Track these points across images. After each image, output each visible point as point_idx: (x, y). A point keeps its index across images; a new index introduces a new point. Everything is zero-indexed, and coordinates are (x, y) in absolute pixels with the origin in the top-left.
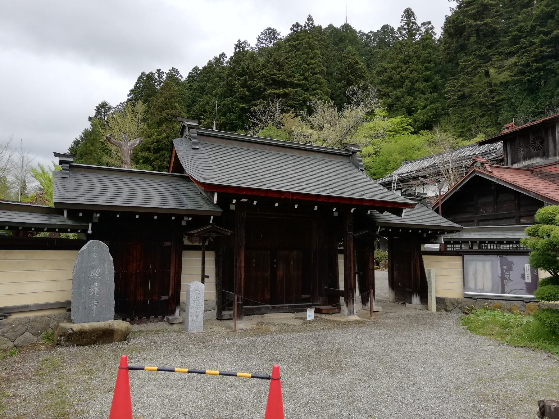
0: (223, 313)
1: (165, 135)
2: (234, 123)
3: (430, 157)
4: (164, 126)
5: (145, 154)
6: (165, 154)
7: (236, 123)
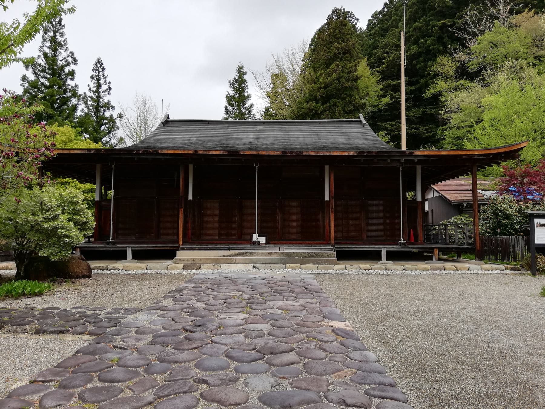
0: (78, 250)
1: (334, 75)
2: (431, 51)
3: (518, 270)
4: (333, 66)
5: (312, 105)
6: (336, 103)
7: (434, 49)
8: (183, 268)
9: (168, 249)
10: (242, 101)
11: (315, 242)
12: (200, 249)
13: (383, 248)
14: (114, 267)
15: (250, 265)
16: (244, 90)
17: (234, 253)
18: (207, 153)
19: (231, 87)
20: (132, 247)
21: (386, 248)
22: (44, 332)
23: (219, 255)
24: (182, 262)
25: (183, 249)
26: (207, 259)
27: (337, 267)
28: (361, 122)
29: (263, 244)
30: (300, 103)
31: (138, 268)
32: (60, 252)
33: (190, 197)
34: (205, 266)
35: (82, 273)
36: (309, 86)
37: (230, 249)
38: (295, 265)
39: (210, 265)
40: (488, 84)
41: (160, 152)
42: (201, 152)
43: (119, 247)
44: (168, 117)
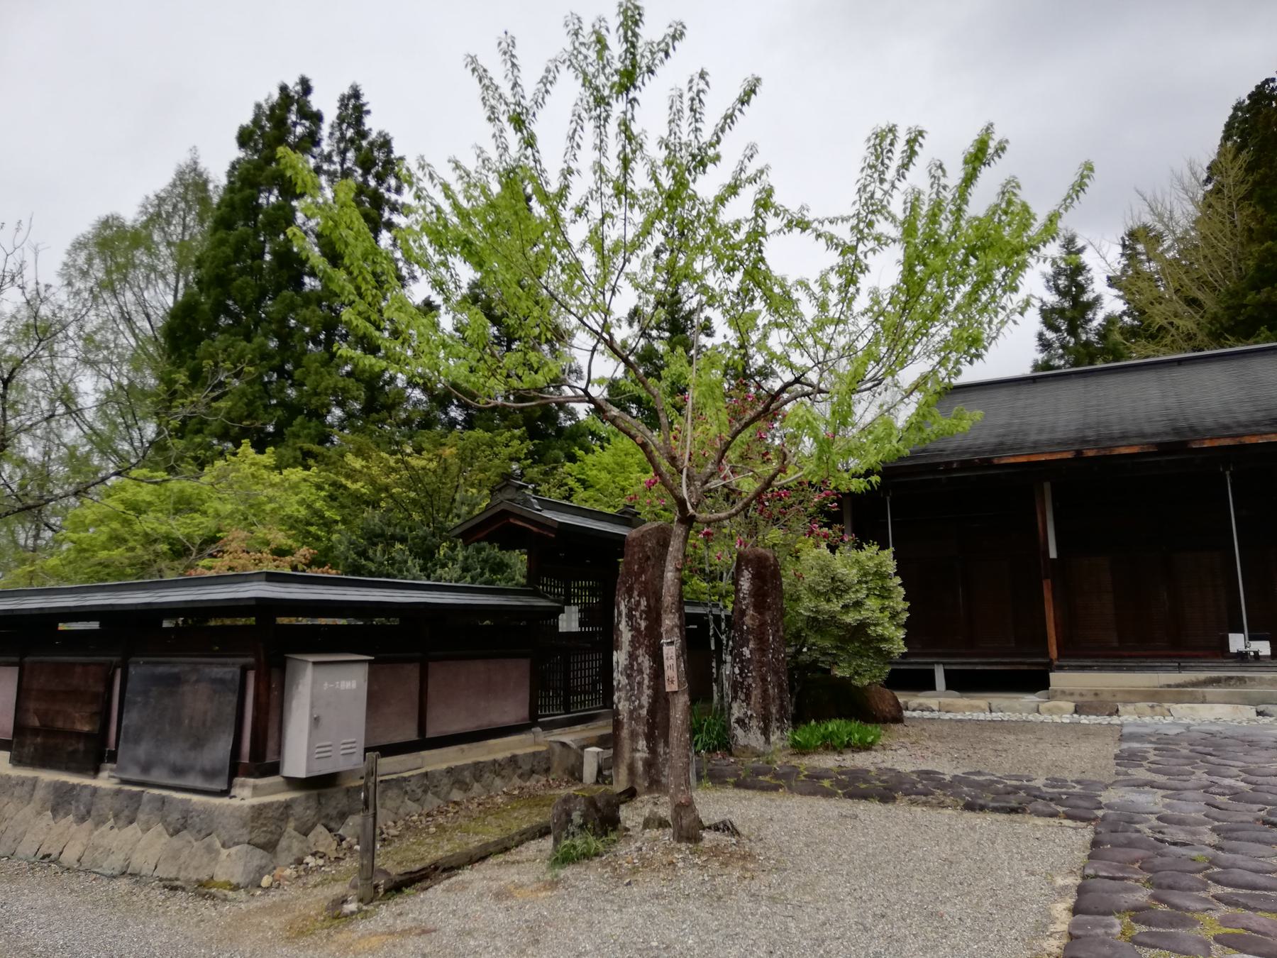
8: (1076, 712)
9: (1025, 667)
10: (1083, 315)
12: (1101, 669)
14: (920, 705)
15: (1248, 707)
16: (1082, 289)
17: (1194, 679)
18: (1107, 453)
19: (1049, 288)
20: (944, 664)
22: (982, 808)
23: (1156, 684)
25: (1060, 668)
26: (1129, 692)
29: (1265, 657)
30: (1232, 294)
31: (973, 708)
32: (871, 671)
34: (1130, 708)
35: (890, 712)
36: (1255, 248)
37: (1180, 669)
39: (1143, 706)
41: (996, 461)
42: (1091, 453)
43: (917, 663)
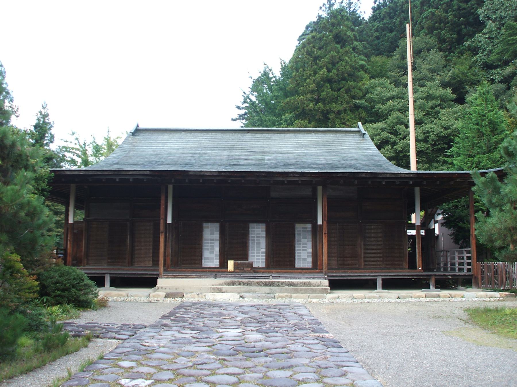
11: (370, 270)
13: (379, 275)
15: (237, 294)
21: (382, 276)
24: (164, 290)
27: (329, 296)
28: (359, 131)
33: (169, 221)
38: (285, 294)
40: (63, 341)
44: (138, 126)
